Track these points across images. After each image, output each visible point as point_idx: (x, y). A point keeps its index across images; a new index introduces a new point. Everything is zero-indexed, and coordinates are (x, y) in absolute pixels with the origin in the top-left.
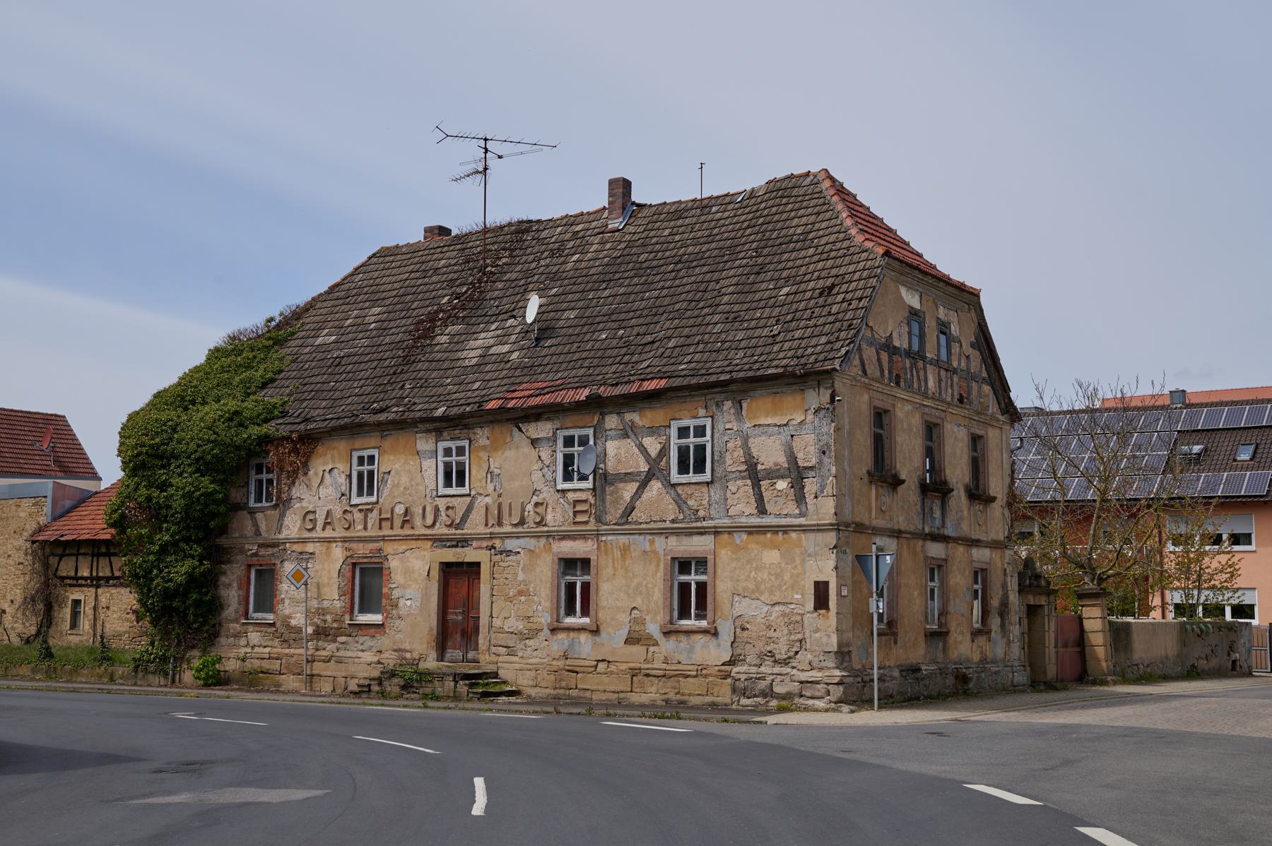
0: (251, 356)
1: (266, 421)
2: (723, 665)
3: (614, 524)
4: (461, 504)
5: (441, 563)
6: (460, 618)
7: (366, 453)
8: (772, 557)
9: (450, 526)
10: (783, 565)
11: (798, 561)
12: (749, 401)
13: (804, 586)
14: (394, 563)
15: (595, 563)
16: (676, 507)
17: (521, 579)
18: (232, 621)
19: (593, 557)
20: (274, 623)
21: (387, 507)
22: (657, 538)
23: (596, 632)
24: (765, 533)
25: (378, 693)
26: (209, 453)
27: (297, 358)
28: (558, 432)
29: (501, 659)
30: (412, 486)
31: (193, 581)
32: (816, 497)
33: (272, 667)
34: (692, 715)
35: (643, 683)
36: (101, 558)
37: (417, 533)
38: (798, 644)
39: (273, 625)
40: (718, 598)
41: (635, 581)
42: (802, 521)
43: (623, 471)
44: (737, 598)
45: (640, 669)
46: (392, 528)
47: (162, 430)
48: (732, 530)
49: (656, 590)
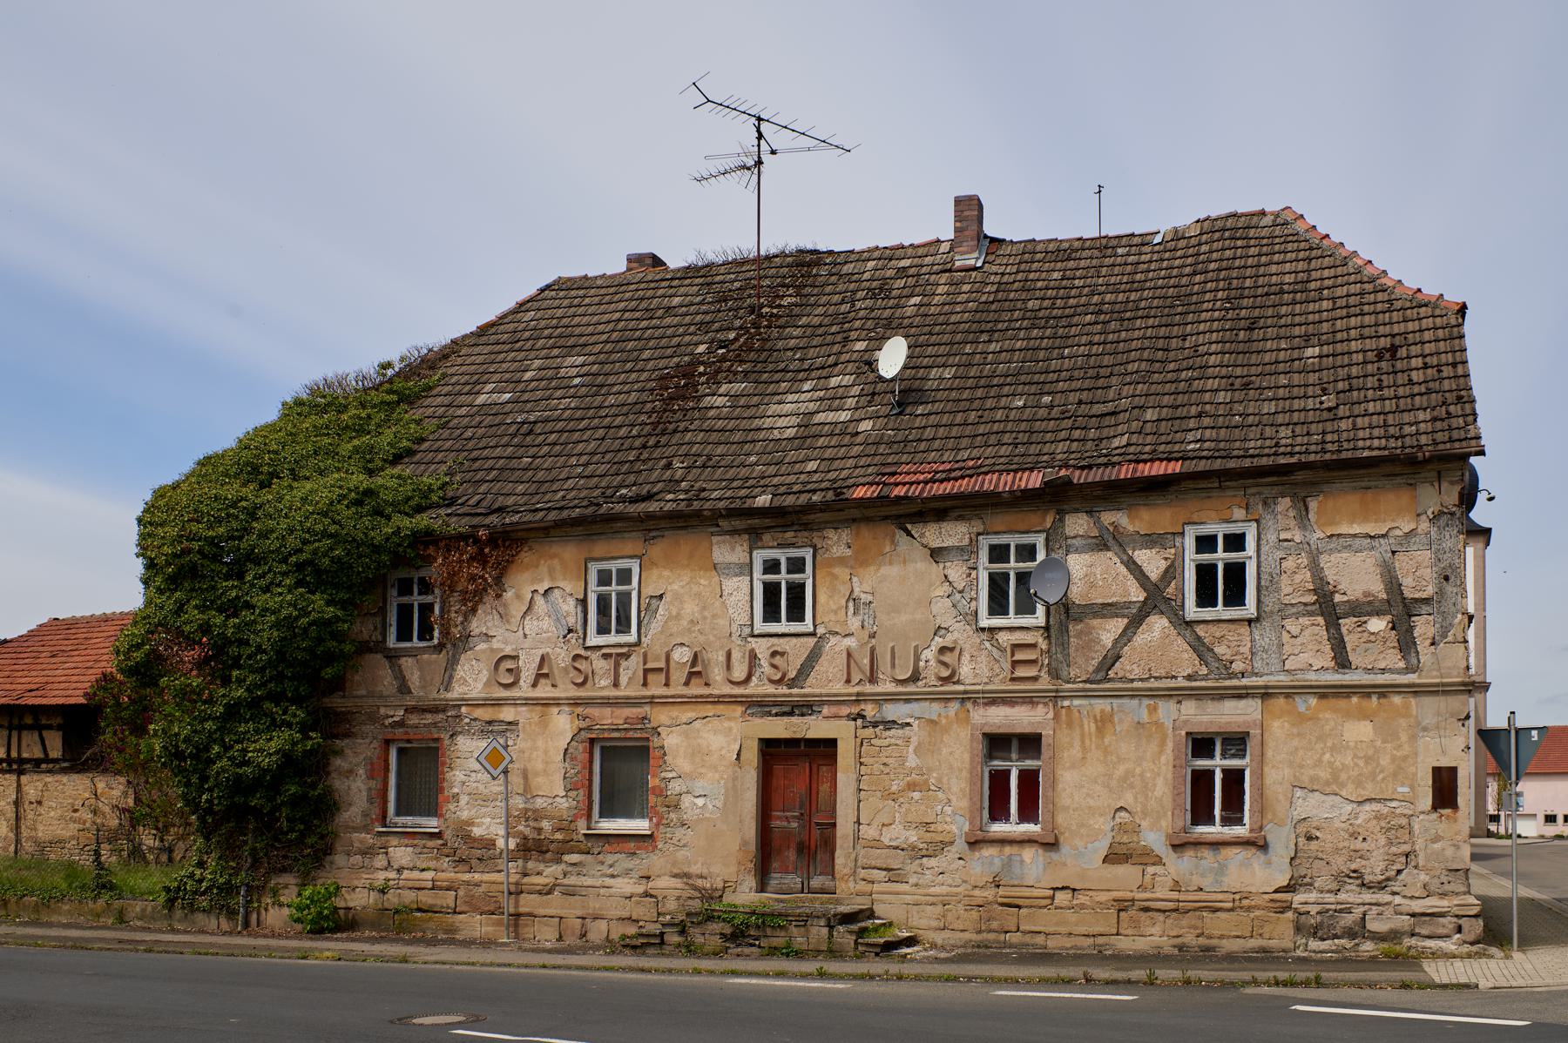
0: (363, 415)
1: (420, 509)
2: (1276, 891)
3: (1084, 682)
4: (797, 651)
5: (760, 739)
6: (796, 825)
7: (614, 566)
8: (1359, 731)
9: (779, 682)
10: (1378, 743)
11: (1404, 737)
12: (1321, 498)
13: (1415, 774)
14: (671, 740)
15: (1051, 741)
16: (1195, 656)
17: (914, 765)
18: (356, 829)
19: (1047, 732)
20: (440, 833)
21: (659, 650)
23: (1052, 845)
24: (1348, 696)
25: (679, 945)
26: (325, 555)
27: (448, 422)
28: (981, 538)
29: (876, 887)
30: (705, 618)
31: (290, 764)
32: (1433, 644)
33: (439, 902)
34: (1271, 974)
35: (1139, 921)
36: (25, 734)
37: (716, 692)
38: (1403, 859)
39: (438, 835)
40: (1268, 792)
41: (1122, 769)
42: (1412, 678)
44: (1299, 793)
45: (1133, 900)
46: (667, 685)
47: (228, 515)
48: (1290, 692)
49: (1160, 782)
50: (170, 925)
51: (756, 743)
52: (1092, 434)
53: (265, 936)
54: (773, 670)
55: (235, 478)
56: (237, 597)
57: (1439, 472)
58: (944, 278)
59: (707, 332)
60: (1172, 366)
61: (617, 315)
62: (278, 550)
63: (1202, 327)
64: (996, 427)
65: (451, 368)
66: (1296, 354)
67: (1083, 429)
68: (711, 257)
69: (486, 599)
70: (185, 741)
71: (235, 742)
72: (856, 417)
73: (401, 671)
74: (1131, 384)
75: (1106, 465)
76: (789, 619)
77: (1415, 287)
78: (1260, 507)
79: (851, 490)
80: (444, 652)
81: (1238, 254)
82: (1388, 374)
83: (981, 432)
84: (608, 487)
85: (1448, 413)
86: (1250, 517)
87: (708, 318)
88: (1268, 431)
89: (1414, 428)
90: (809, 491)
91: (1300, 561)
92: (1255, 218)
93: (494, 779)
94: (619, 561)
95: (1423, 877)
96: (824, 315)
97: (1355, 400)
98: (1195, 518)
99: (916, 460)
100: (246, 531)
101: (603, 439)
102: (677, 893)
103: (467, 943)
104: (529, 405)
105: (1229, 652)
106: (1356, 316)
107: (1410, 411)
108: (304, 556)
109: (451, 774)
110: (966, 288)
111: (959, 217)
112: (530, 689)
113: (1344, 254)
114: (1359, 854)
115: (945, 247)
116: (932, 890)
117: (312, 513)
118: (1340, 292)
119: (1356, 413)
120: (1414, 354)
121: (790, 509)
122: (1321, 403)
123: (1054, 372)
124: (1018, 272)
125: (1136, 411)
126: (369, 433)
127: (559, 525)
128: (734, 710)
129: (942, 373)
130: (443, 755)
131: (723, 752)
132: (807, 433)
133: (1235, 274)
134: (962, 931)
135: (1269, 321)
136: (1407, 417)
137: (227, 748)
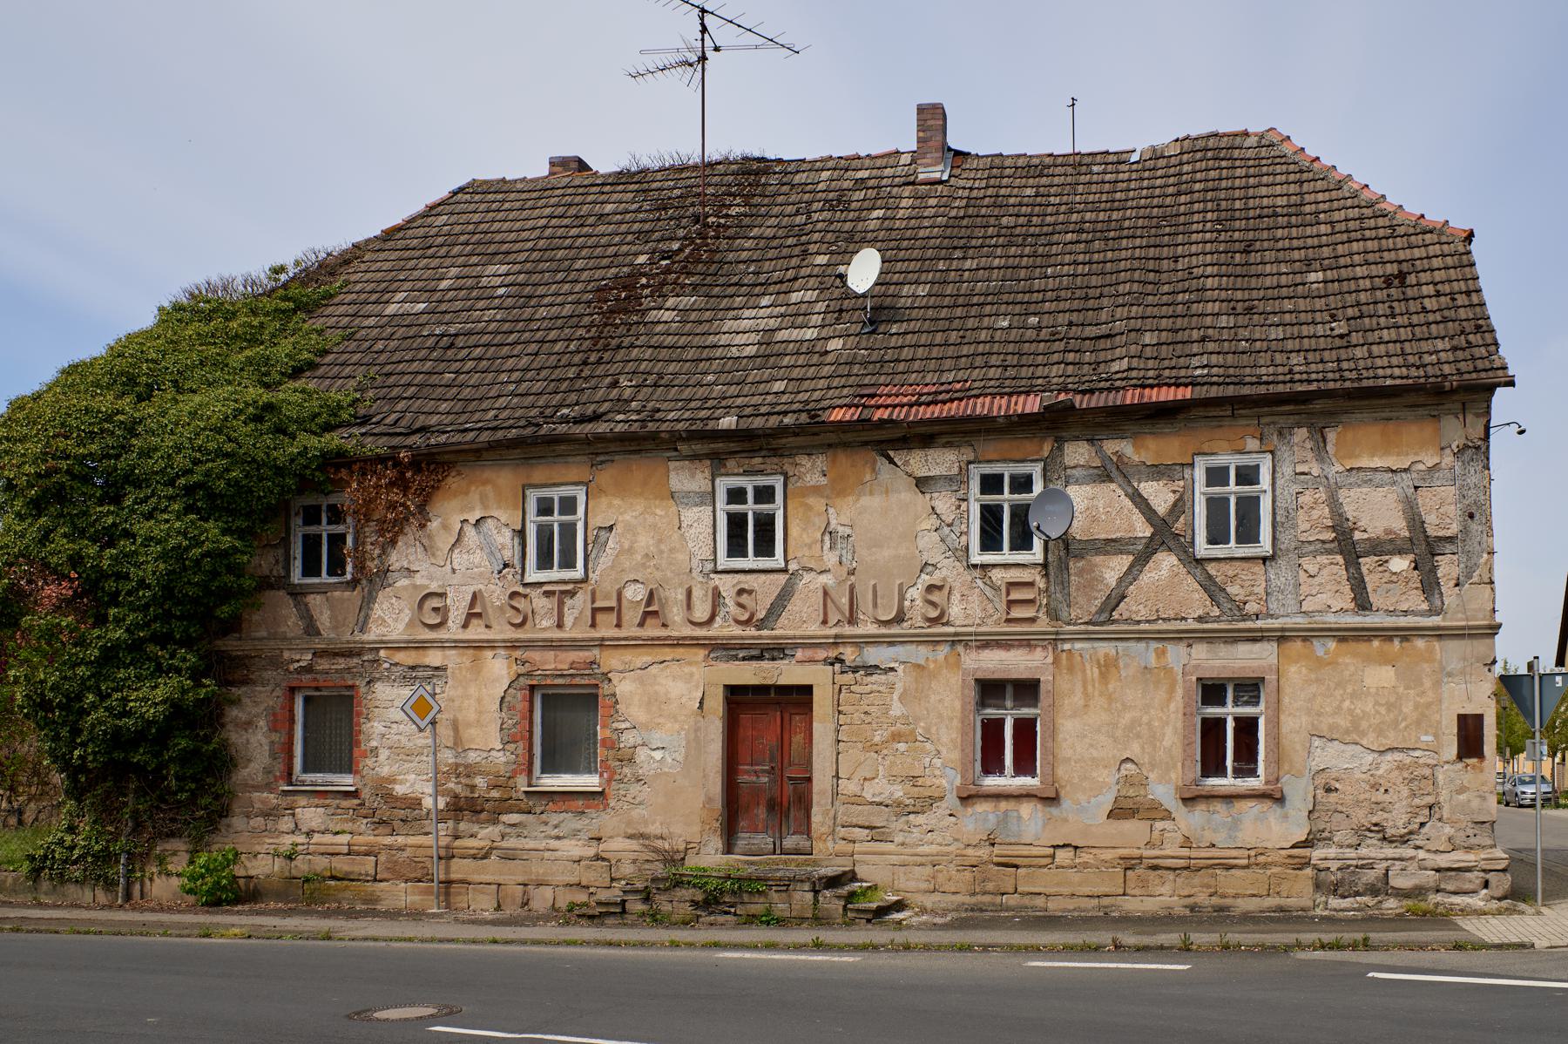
0: (255, 323)
1: (328, 428)
2: (1293, 847)
4: (768, 588)
5: (725, 686)
7: (556, 494)
8: (1381, 677)
9: (747, 622)
10: (1401, 689)
11: (1428, 683)
12: (1340, 429)
13: (1439, 722)
14: (624, 687)
15: (1050, 688)
17: (898, 713)
18: (257, 788)
19: (1045, 677)
20: (356, 791)
22: (1170, 647)
23: (1051, 800)
24: (1369, 639)
28: (971, 466)
30: (662, 552)
31: (179, 715)
32: (1457, 585)
33: (356, 869)
35: (1148, 881)
38: (1426, 812)
40: (1285, 742)
43: (1103, 536)
44: (1317, 742)
45: (1141, 858)
46: (618, 625)
47: (102, 431)
48: (1308, 635)
49: (1169, 731)
50: (35, 899)
51: (721, 689)
52: (1087, 357)
53: (153, 910)
54: (739, 610)
55: (108, 388)
56: (114, 525)
57: (1464, 404)
58: (907, 191)
59: (647, 242)
60: (1166, 288)
61: (543, 222)
62: (163, 471)
63: (1194, 249)
64: (981, 348)
65: (355, 272)
66: (1298, 279)
67: (1076, 352)
68: (646, 162)
69: (407, 529)
70: (52, 689)
71: (113, 689)
72: (823, 335)
73: (308, 610)
74: (1124, 306)
75: (1109, 390)
76: (757, 554)
77: (1418, 213)
78: (1275, 437)
79: (827, 412)
80: (359, 588)
81: (1224, 175)
82: (1399, 301)
83: (964, 353)
84: (547, 407)
85: (1468, 342)
86: (1264, 448)
87: (647, 227)
88: (1279, 358)
89: (1434, 357)
90: (779, 413)
91: (1317, 496)
92: (1238, 139)
93: (421, 730)
94: (562, 488)
95: (1448, 830)
96: (778, 226)
97: (1368, 327)
98: (1206, 448)
99: (896, 381)
100: (125, 448)
101: (536, 354)
102: (633, 856)
103: (393, 915)
104: (448, 317)
105: (1242, 592)
106: (1358, 241)
107: (1427, 339)
108: (195, 478)
109: (369, 725)
110: (932, 202)
111: (922, 126)
112: (460, 630)
113: (1338, 178)
114: (1381, 806)
115: (906, 159)
116: (920, 849)
117: (204, 429)
118: (1337, 216)
119: (1370, 340)
120: (1424, 281)
121: (761, 432)
122: (1332, 329)
123: (1038, 291)
124: (987, 187)
125: (1133, 334)
126: (262, 343)
127: (493, 446)
128: (696, 654)
129: (915, 290)
130: (360, 704)
131: (683, 700)
132: (769, 352)
133: (1222, 195)
134: (954, 893)
135: (1266, 244)
136: (1425, 346)
137: (104, 697)
